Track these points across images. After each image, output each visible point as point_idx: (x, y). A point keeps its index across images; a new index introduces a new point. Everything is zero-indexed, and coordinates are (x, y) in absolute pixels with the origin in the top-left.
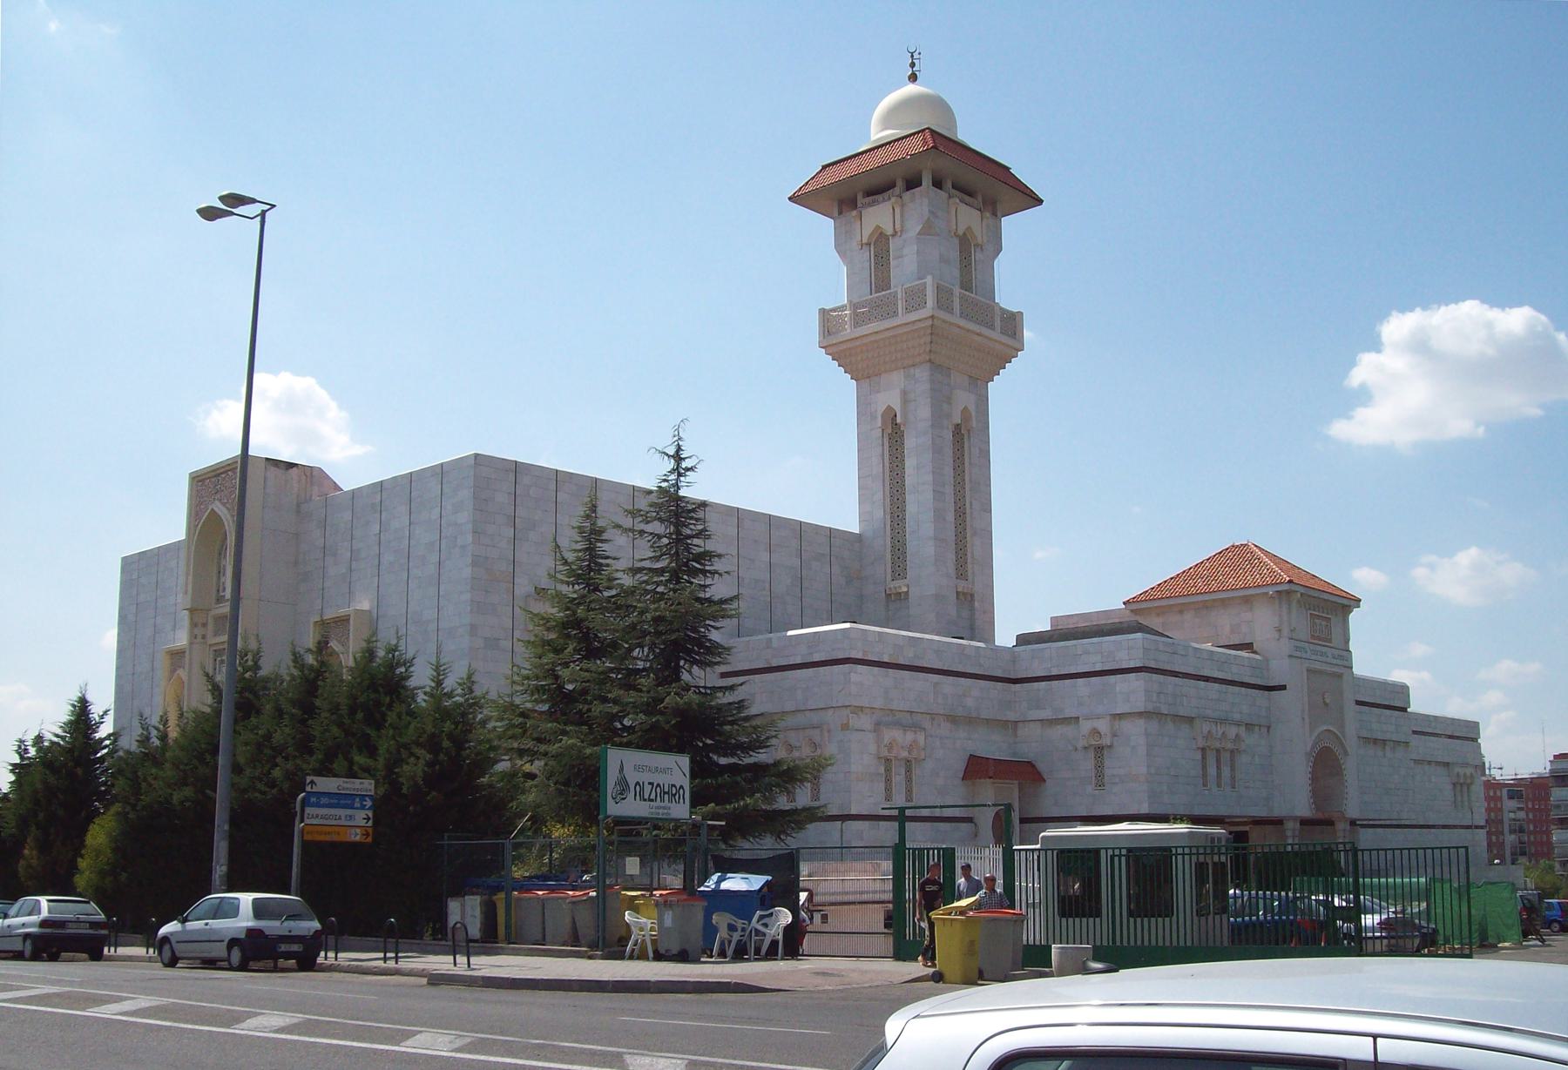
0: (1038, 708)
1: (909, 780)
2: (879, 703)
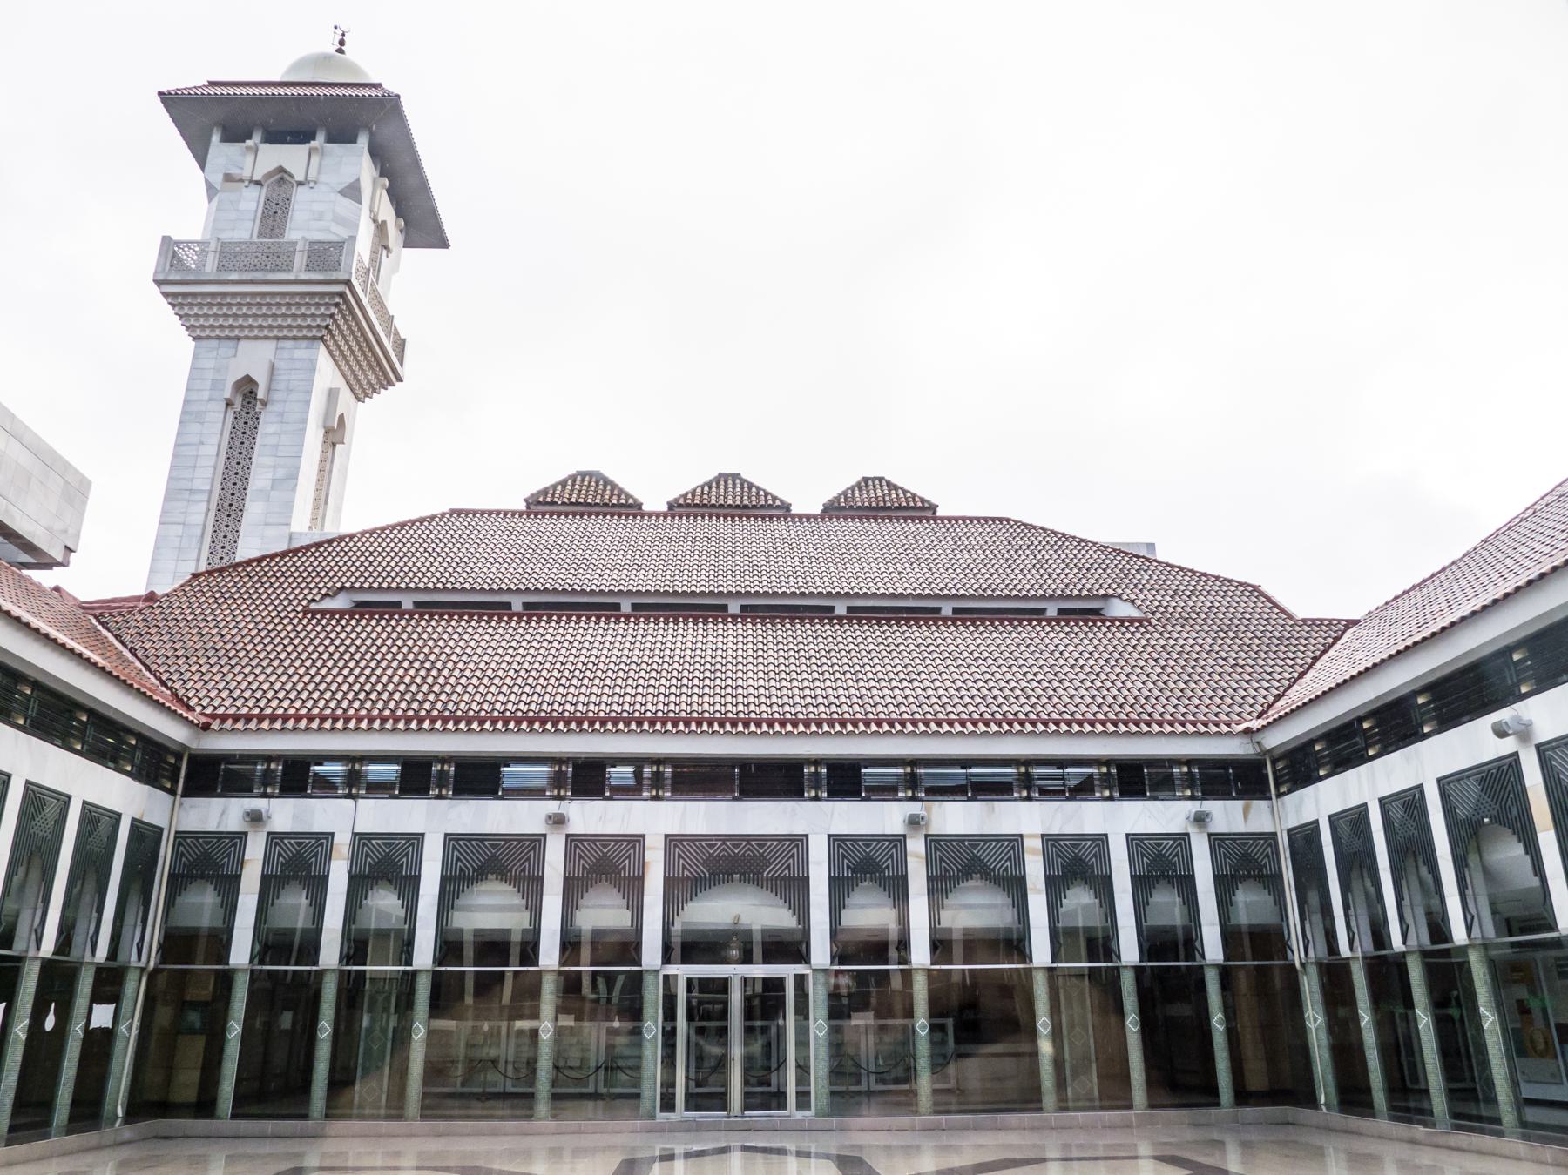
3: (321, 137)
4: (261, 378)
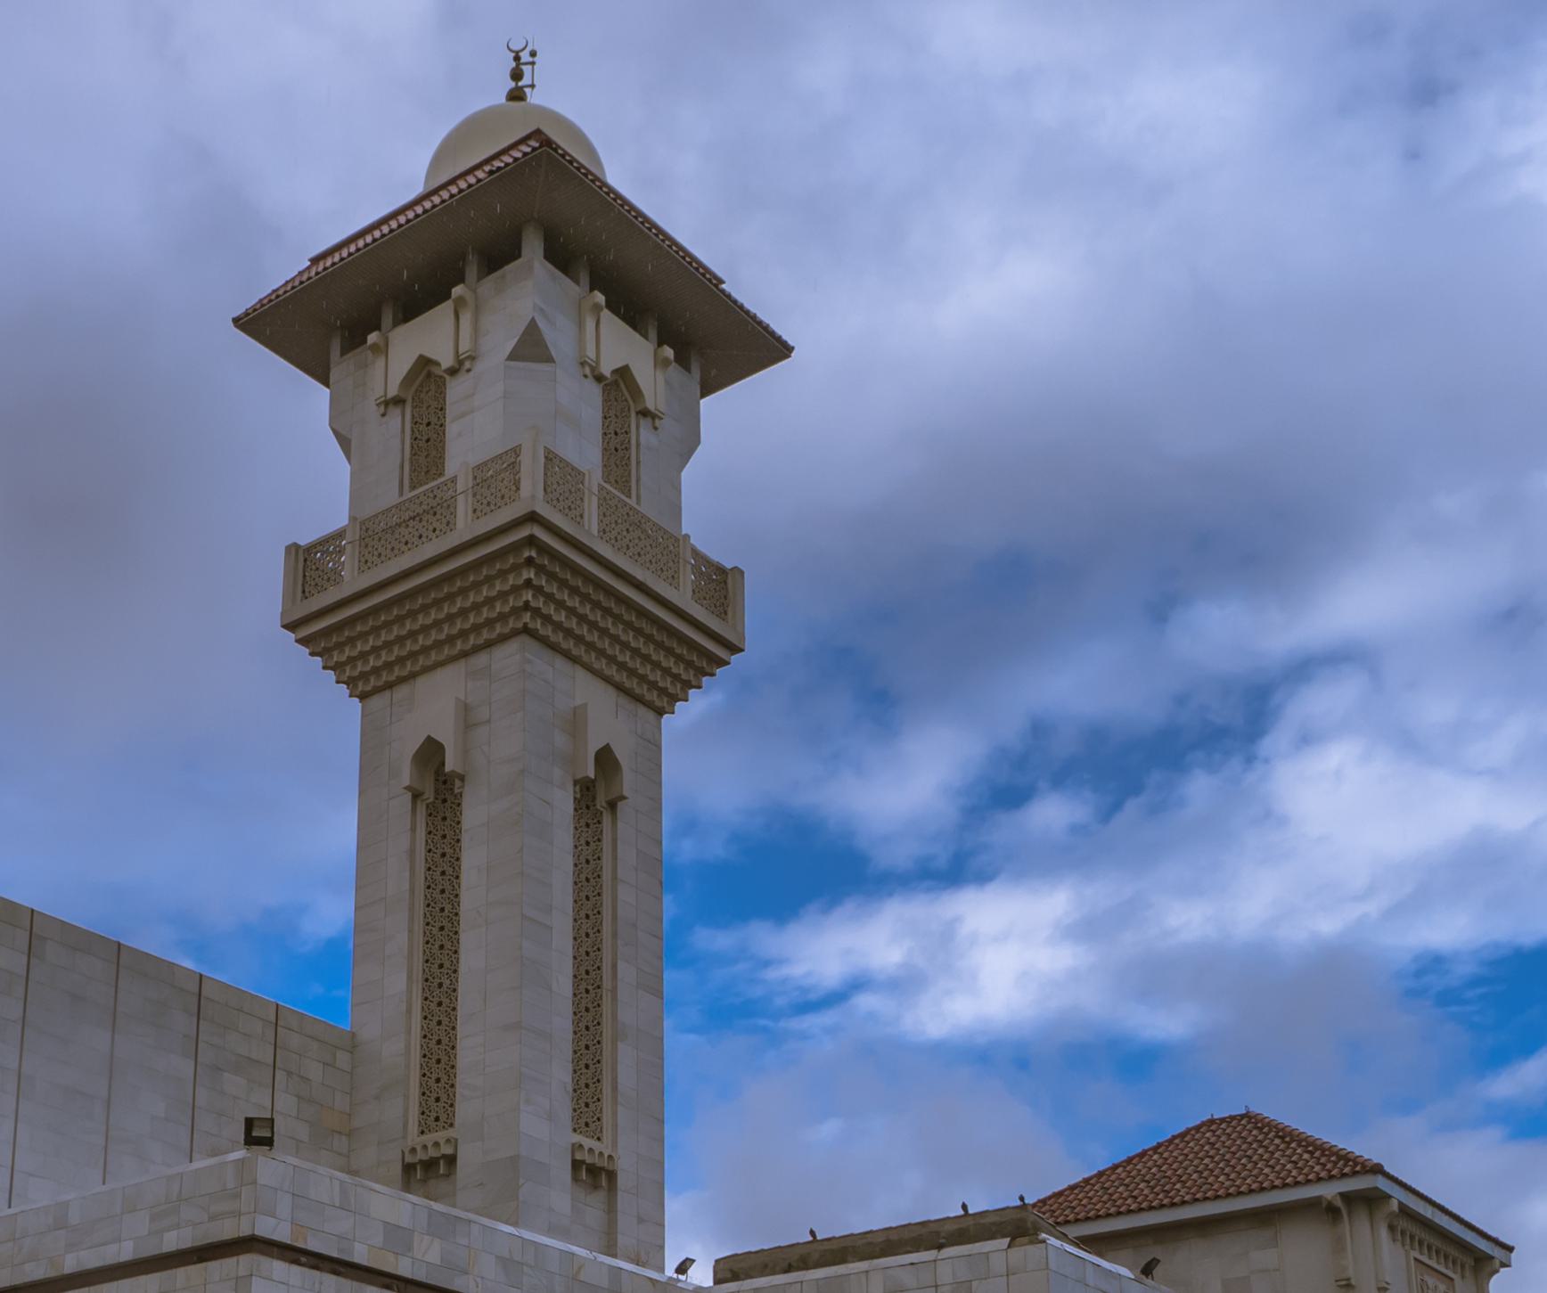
3: (472, 272)
4: (447, 736)
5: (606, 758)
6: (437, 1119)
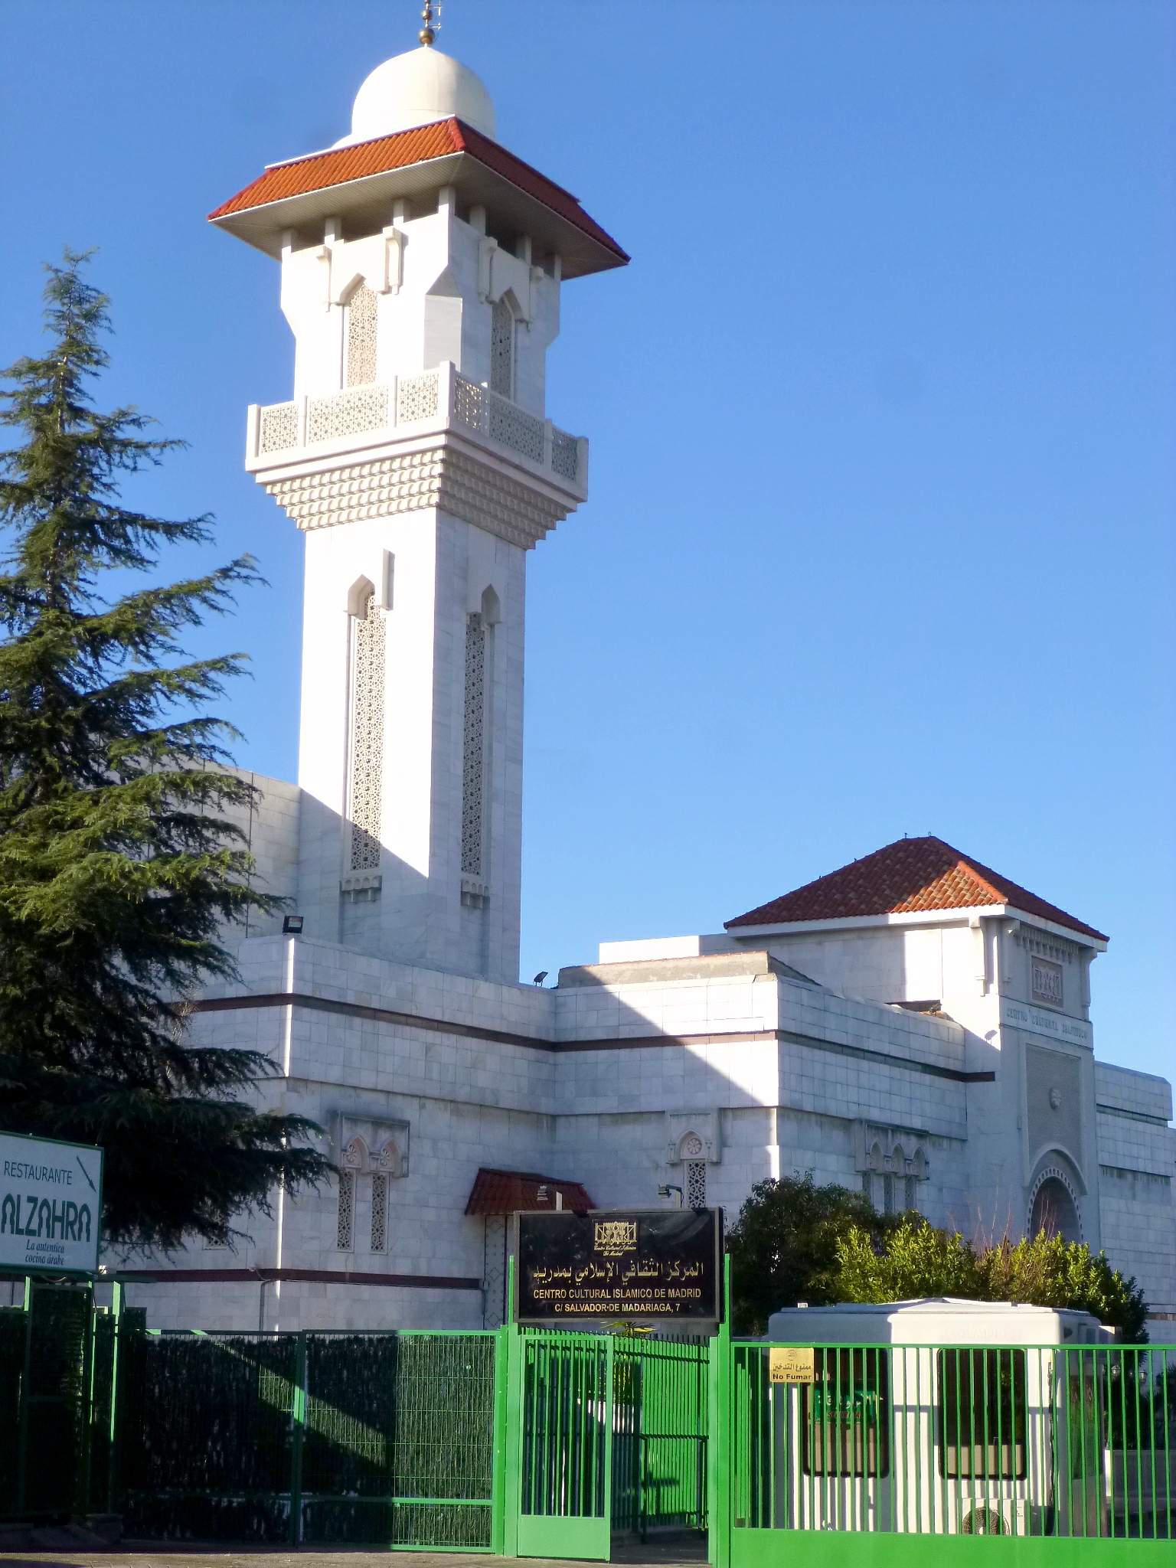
0: (595, 1093)
1: (379, 1212)
2: (334, 1075)
5: (489, 595)
6: (366, 859)
